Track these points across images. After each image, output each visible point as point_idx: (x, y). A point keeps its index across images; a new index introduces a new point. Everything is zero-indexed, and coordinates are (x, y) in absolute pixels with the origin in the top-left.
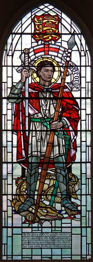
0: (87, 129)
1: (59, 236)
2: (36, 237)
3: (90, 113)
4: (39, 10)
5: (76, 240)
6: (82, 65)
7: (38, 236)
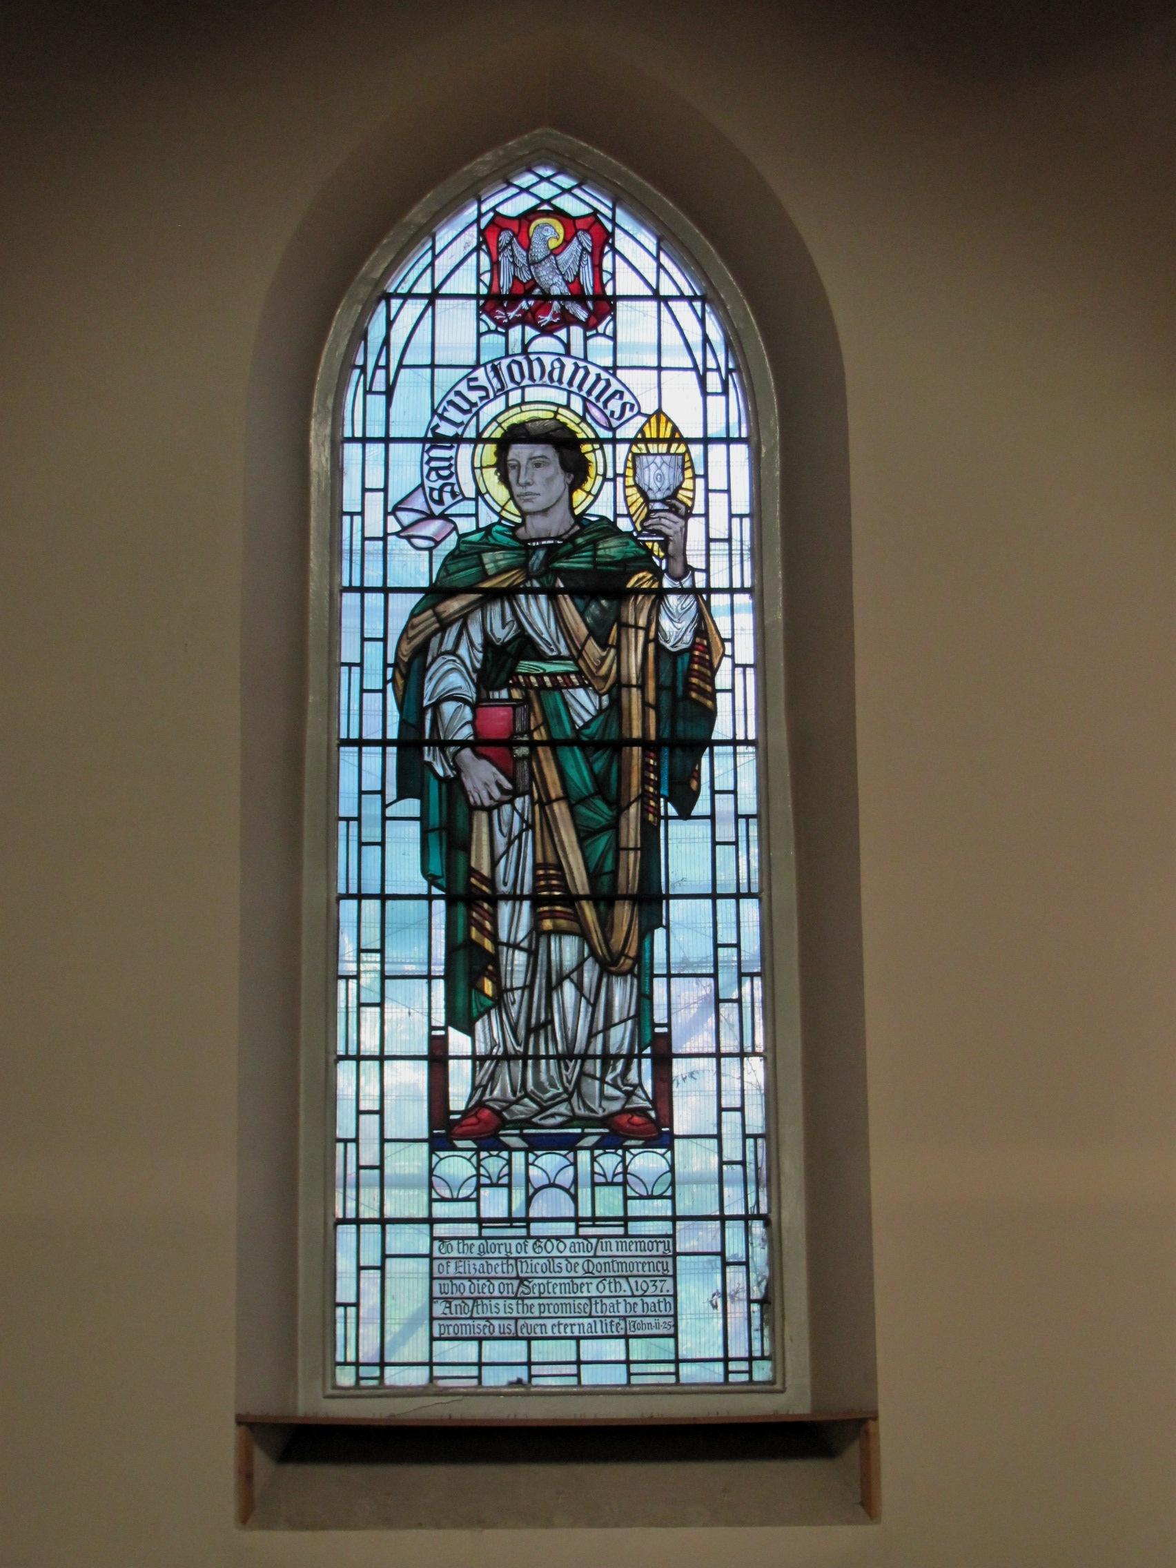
0: (737, 584)
1: (615, 1253)
2: (499, 1262)
3: (746, 510)
4: (514, 191)
5: (696, 1289)
6: (731, 1354)
7: (508, 1258)
